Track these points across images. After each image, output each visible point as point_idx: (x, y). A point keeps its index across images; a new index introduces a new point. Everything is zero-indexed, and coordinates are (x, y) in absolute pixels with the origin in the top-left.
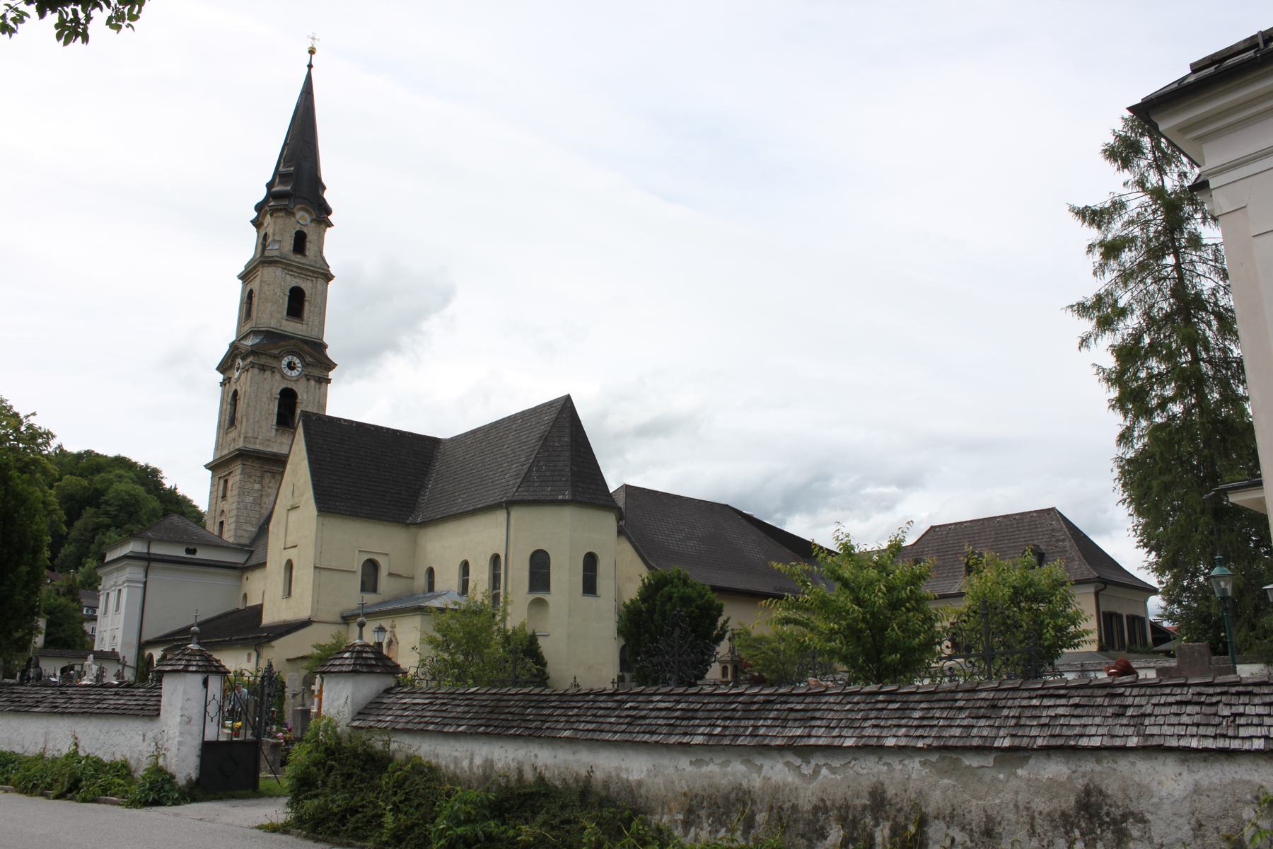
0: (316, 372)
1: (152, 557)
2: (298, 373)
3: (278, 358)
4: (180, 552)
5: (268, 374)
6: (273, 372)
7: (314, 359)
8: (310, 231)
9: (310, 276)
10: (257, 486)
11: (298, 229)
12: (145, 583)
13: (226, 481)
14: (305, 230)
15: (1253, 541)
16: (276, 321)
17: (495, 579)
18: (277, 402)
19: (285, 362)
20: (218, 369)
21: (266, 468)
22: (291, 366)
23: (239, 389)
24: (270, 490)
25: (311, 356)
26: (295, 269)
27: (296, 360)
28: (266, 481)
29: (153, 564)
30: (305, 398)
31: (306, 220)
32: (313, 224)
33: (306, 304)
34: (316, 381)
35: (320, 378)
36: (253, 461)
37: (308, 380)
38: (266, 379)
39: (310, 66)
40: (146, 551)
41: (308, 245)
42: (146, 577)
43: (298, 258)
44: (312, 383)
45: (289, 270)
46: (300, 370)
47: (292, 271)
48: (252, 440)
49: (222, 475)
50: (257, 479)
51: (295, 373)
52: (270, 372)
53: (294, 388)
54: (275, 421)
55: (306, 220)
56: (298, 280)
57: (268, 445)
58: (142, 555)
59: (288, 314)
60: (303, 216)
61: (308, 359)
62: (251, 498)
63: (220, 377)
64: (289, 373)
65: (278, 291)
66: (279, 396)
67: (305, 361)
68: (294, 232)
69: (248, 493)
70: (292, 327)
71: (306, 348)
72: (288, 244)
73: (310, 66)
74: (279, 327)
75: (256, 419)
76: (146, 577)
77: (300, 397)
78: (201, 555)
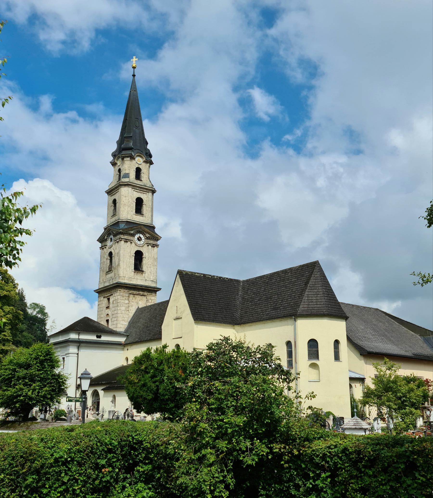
0: (152, 242)
1: (81, 340)
2: (143, 243)
3: (133, 235)
4: (93, 338)
5: (129, 243)
6: (131, 243)
7: (150, 235)
8: (144, 167)
9: (145, 191)
10: (127, 302)
11: (137, 166)
12: (78, 354)
13: (109, 299)
14: (140, 167)
15: (244, 371)
16: (130, 216)
17: (290, 354)
18: (134, 258)
19: (137, 236)
20: (98, 240)
21: (131, 292)
22: (139, 239)
23: (113, 251)
24: (133, 303)
25: (149, 233)
26: (137, 188)
27: (142, 236)
28: (131, 298)
29: (82, 345)
30: (147, 255)
31: (140, 161)
32: (144, 164)
33: (144, 206)
34: (152, 246)
35: (153, 244)
36: (124, 289)
37: (148, 246)
38: (128, 246)
39: (134, 76)
40: (78, 338)
41: (142, 175)
42: (78, 351)
43: (138, 182)
44: (150, 247)
45: (135, 189)
46: (144, 241)
47: (136, 189)
48: (123, 278)
49: (106, 296)
50: (127, 298)
51: (142, 242)
52: (129, 243)
53: (141, 250)
54: (133, 268)
55: (140, 161)
56: (139, 194)
57: (131, 280)
58: (76, 340)
59: (309, 359)
60: (139, 159)
61: (148, 235)
62: (124, 308)
63: (100, 245)
64: (139, 242)
65: (130, 200)
66: (134, 255)
67: (146, 236)
68: (135, 168)
69: (123, 305)
70: (138, 219)
71: (146, 230)
72: (133, 175)
73: (134, 76)
74: (132, 219)
75: (124, 267)
76: (78, 351)
77: (144, 255)
78: (104, 338)
